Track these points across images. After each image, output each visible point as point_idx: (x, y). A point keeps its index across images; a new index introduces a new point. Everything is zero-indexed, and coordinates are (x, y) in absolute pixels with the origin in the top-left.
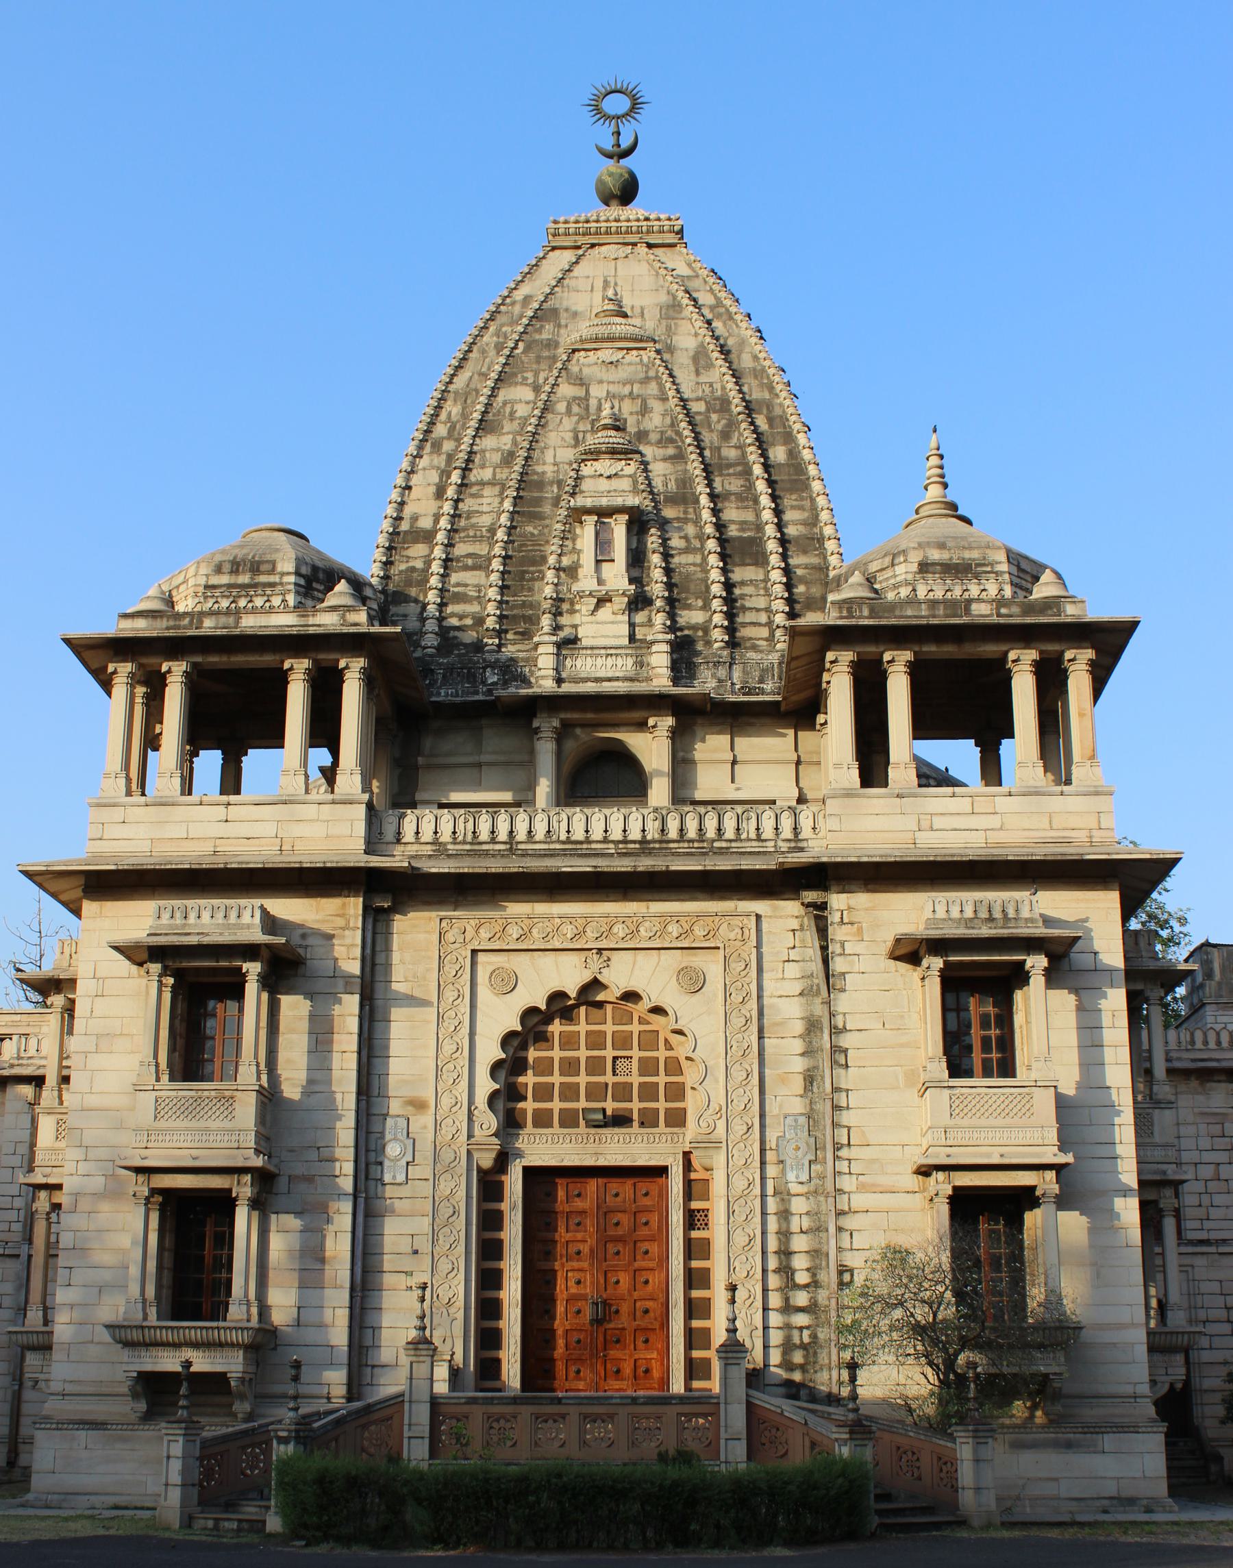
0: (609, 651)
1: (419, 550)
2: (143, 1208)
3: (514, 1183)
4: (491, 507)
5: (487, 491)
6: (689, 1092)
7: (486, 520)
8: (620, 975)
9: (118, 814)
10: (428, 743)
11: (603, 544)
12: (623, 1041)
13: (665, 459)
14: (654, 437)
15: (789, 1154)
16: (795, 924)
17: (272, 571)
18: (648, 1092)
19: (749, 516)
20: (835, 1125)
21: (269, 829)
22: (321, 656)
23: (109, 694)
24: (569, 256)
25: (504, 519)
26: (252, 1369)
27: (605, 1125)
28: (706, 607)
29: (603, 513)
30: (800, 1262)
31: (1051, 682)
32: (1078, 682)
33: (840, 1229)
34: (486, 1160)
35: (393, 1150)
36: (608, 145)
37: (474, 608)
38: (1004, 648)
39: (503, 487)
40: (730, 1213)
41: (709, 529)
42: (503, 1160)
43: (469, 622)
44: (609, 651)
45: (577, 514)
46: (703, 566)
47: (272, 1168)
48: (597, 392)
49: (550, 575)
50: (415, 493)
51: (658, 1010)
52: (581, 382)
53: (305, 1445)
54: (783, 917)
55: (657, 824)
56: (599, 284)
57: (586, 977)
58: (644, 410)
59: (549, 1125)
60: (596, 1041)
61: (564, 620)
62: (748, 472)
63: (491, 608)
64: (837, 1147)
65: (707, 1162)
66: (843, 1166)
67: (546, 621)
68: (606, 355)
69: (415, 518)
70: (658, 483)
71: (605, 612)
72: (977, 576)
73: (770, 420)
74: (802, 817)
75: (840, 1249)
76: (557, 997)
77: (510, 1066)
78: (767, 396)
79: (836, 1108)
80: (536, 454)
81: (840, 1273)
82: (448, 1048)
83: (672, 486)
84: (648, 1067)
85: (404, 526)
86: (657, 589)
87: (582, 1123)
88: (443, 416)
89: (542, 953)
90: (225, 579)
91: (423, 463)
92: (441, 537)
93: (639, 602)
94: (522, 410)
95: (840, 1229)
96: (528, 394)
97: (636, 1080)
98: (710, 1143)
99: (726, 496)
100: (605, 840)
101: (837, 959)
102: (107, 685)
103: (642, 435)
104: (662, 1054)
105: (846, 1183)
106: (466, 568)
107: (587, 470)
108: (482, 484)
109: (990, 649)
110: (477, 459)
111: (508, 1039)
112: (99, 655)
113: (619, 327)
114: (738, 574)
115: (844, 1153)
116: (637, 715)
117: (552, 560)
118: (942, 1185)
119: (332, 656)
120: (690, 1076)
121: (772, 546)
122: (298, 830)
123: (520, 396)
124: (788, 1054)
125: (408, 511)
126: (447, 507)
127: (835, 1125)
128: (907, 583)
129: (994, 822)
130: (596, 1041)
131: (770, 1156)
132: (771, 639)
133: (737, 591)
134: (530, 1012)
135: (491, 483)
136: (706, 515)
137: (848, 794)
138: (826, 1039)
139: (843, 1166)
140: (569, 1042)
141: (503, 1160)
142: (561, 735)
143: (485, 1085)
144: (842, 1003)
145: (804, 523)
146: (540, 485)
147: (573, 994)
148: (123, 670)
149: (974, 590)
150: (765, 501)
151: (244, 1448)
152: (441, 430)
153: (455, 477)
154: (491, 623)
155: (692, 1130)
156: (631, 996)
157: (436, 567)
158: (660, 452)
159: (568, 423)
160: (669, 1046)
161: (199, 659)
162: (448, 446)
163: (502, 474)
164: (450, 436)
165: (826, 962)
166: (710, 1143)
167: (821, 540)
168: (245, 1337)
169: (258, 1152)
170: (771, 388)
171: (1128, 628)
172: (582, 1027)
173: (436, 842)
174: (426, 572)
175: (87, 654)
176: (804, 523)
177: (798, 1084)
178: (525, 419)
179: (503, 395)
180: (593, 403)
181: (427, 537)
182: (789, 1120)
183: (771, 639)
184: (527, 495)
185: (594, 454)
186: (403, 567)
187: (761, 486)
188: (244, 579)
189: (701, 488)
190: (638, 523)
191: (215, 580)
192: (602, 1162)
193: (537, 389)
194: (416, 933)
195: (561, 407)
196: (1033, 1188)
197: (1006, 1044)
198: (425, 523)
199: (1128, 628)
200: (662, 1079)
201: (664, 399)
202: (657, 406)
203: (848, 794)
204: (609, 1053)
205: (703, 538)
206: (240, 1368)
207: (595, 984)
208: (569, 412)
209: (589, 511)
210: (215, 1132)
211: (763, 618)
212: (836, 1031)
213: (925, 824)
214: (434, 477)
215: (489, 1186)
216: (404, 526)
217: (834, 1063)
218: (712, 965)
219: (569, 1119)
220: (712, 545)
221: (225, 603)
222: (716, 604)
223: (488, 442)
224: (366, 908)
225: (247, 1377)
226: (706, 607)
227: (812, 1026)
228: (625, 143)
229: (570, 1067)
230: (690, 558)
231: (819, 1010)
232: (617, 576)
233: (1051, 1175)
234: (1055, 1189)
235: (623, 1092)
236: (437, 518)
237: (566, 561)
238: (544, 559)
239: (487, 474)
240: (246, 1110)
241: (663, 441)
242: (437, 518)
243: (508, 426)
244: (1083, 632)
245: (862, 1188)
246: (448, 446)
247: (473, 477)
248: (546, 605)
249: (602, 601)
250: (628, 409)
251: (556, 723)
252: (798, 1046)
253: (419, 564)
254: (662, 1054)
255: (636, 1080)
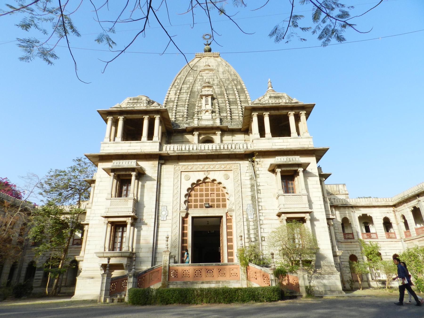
0: (208, 120)
1: (172, 104)
2: (106, 226)
3: (189, 220)
4: (185, 96)
5: (185, 94)
6: (227, 200)
7: (184, 99)
8: (212, 176)
9: (107, 145)
10: (173, 138)
11: (207, 101)
12: (213, 190)
13: (218, 88)
14: (216, 85)
15: (249, 212)
16: (248, 165)
17: (141, 100)
18: (218, 200)
19: (234, 97)
20: (259, 206)
21: (139, 148)
22: (151, 115)
23: (107, 123)
24: (199, 59)
25: (188, 98)
26: (129, 263)
27: (209, 207)
28: (226, 113)
29: (207, 96)
30: (252, 236)
31: (297, 119)
32: (303, 117)
33: (261, 228)
34: (184, 215)
35: (164, 213)
36: (206, 43)
37: (182, 114)
38: (287, 111)
39: (188, 93)
40: (237, 225)
41: (227, 99)
42: (187, 215)
43: (181, 116)
44: (208, 120)
45: (201, 97)
46: (226, 106)
47: (136, 216)
48: (204, 77)
49: (197, 107)
50: (171, 94)
51: (220, 183)
52: (202, 76)
53: (136, 278)
54: (245, 164)
55: (219, 146)
56: (205, 62)
57: (205, 176)
58: (214, 80)
59: (197, 208)
60: (207, 190)
61: (199, 115)
62: (234, 91)
63: (185, 113)
64: (259, 210)
65: (231, 215)
66: (261, 214)
67: (196, 115)
68: (207, 72)
69: (171, 98)
70: (216, 92)
71: (207, 113)
72: (281, 98)
73: (237, 82)
74: (248, 145)
75: (261, 233)
76: (199, 181)
77: (188, 195)
78: (236, 78)
79: (259, 202)
80: (193, 88)
81: (262, 238)
82: (176, 191)
83: (219, 92)
84: (218, 195)
85: (169, 100)
86: (217, 110)
87: (204, 207)
88: (176, 82)
89: (196, 171)
90: (132, 101)
91: (173, 89)
92: (176, 101)
93: (213, 112)
94: (191, 81)
95: (261, 228)
96: (193, 78)
97: (215, 198)
98: (232, 210)
99: (229, 94)
100: (208, 150)
101: (257, 171)
102: (106, 121)
103: (213, 84)
104: (221, 192)
105: (262, 218)
106: (181, 107)
107: (203, 90)
108: (183, 92)
109: (284, 112)
110: (183, 89)
111: (188, 189)
112: (105, 114)
113: (208, 67)
114: (232, 107)
115: (261, 211)
116: (213, 131)
117: (197, 105)
118: (284, 217)
119: (153, 115)
120: (227, 196)
121: (239, 102)
122: (145, 148)
123: (191, 79)
124: (248, 192)
125: (170, 97)
126: (177, 96)
127: (259, 206)
128: (267, 100)
129: (288, 144)
130: (207, 190)
131: (244, 213)
132: (239, 118)
133: (232, 110)
134: (193, 184)
135: (186, 92)
136: (226, 97)
137: (258, 139)
138: (255, 188)
139: (261, 214)
140: (201, 190)
141: (187, 215)
142: (199, 135)
143: (183, 199)
144: (259, 180)
145: (244, 98)
146: (194, 92)
147: (202, 180)
148: (110, 118)
149: (281, 101)
150: (237, 94)
151: (123, 281)
152: (176, 84)
153: (179, 91)
154: (185, 116)
155: (227, 208)
156: (214, 180)
157: (175, 106)
158: (217, 87)
159: (199, 83)
160: (222, 191)
161: (126, 116)
162: (177, 87)
163: (187, 91)
164: (177, 85)
165: (255, 172)
166: (232, 210)
167: (248, 101)
168: (128, 255)
169: (133, 212)
170: (237, 77)
171: (312, 106)
172: (204, 187)
173: (174, 150)
174: (173, 108)
175: (103, 115)
176: (244, 98)
177: (250, 198)
178: (192, 82)
179: (187, 79)
180: (204, 79)
181: (173, 102)
182: (249, 205)
183: (239, 118)
184: (192, 93)
185: (205, 87)
186: (168, 107)
187: (236, 92)
188: (136, 101)
189: (225, 92)
190: (213, 99)
191: (130, 101)
192: (209, 215)
193: (194, 77)
194: (168, 169)
195: (198, 80)
196: (304, 217)
197: (293, 189)
198: (173, 99)
199: (312, 106)
200: (221, 198)
201: (217, 78)
202: (216, 80)
203: (258, 139)
204: (210, 192)
205: (225, 101)
206: (126, 262)
207: (207, 178)
208: (200, 81)
209: (204, 95)
210: (124, 208)
211: (237, 115)
212: (258, 186)
213: (274, 144)
214: (175, 92)
215: (184, 221)
216: (169, 100)
217: (258, 193)
218: (230, 174)
219: (201, 206)
220: (227, 102)
221: (131, 106)
222: (229, 112)
223: (185, 86)
224: (159, 163)
225: (128, 265)
226: (226, 113)
227: (252, 186)
228: (209, 43)
229: (201, 195)
230: (223, 104)
231: (253, 182)
232: (209, 107)
233: (308, 214)
234: (310, 217)
235: (213, 200)
236: (175, 98)
237: (199, 105)
238: (195, 105)
239: (184, 91)
240: (130, 204)
241: (217, 85)
242: (175, 98)
243: (188, 83)
244: (303, 108)
245: (265, 219)
246: (177, 87)
247: (182, 91)
248: (196, 112)
249: (207, 111)
250: (211, 80)
251: (198, 133)
252: (250, 190)
253: (172, 106)
254: (221, 192)
255: (215, 198)
